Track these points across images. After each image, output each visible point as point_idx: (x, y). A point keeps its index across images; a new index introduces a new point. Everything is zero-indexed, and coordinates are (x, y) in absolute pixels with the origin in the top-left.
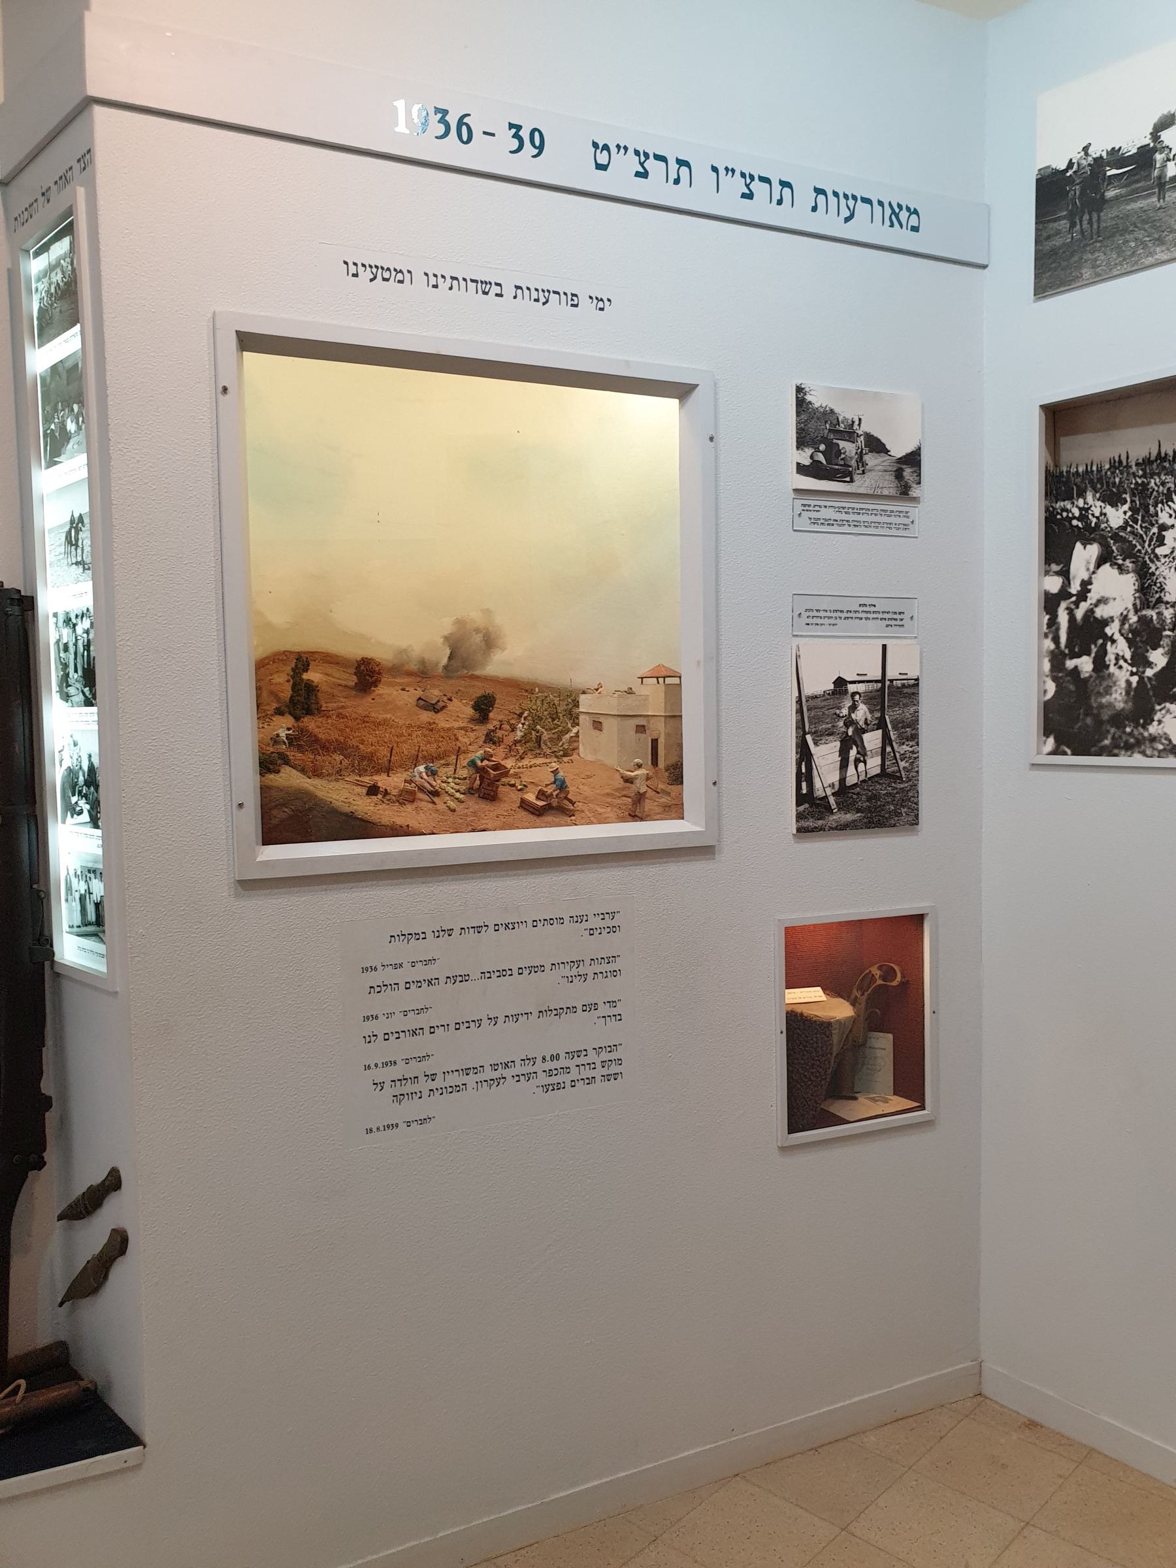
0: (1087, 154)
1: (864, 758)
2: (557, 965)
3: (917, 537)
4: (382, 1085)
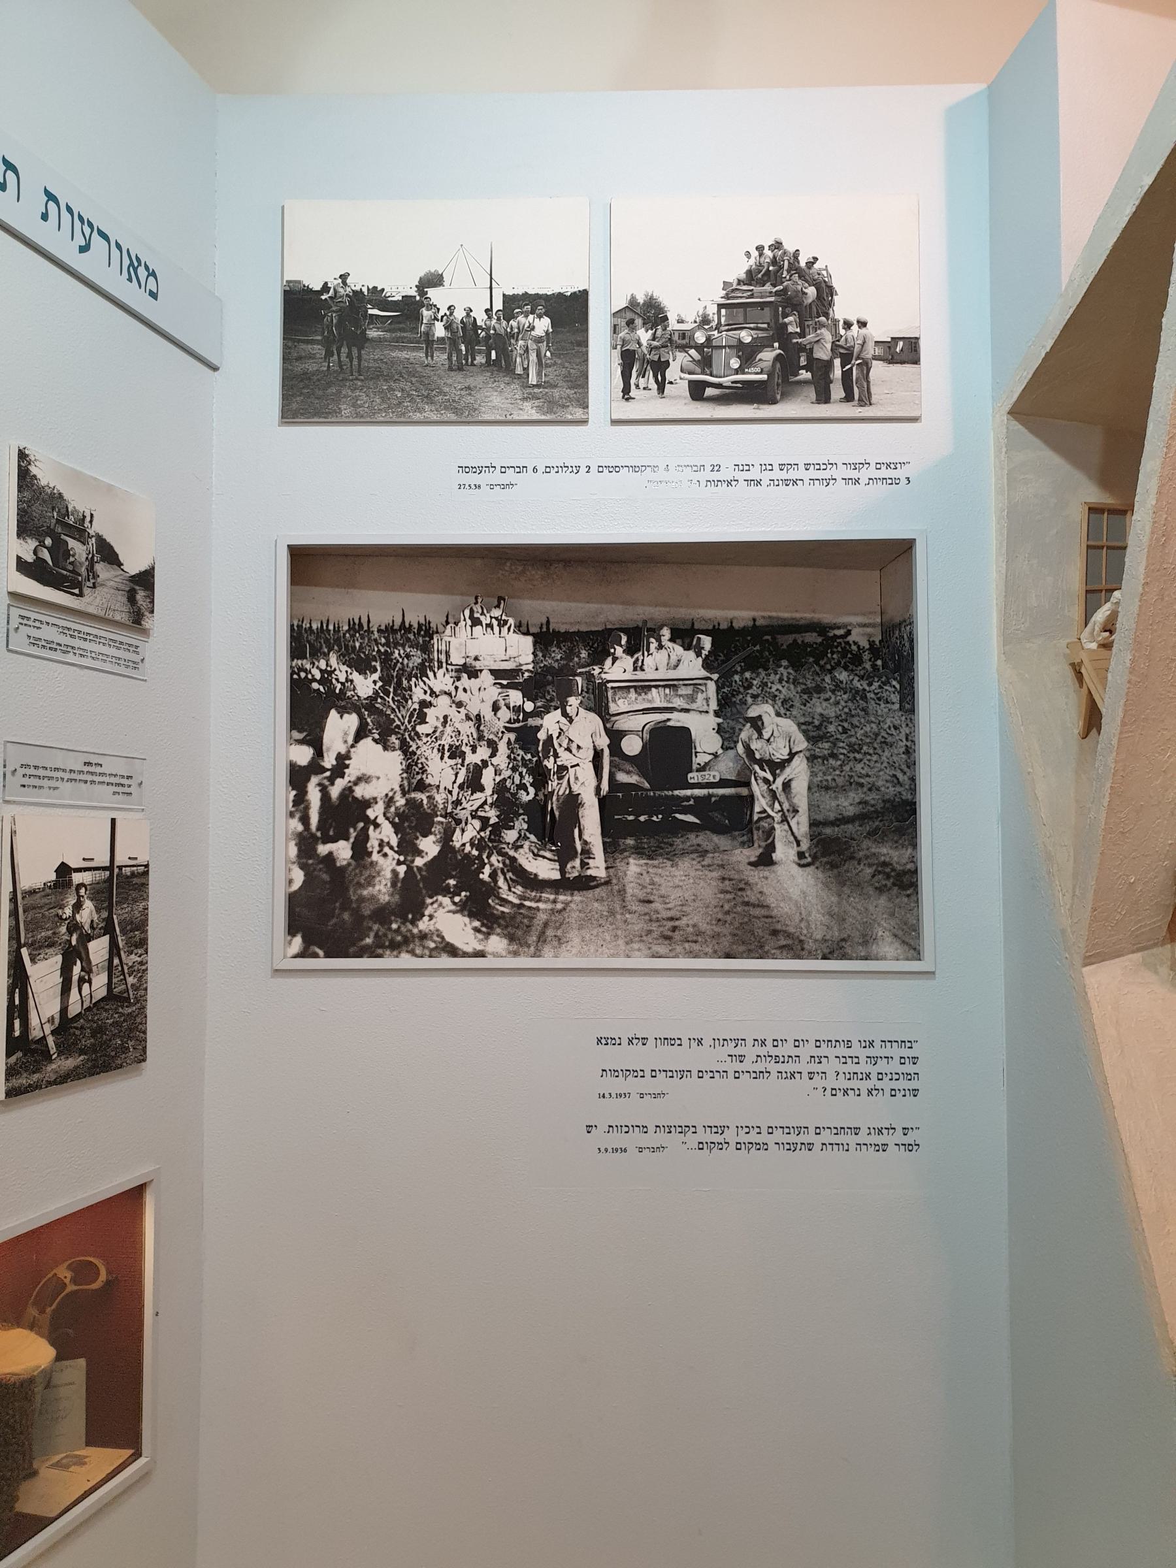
0: (344, 283)
1: (89, 976)
3: (146, 680)
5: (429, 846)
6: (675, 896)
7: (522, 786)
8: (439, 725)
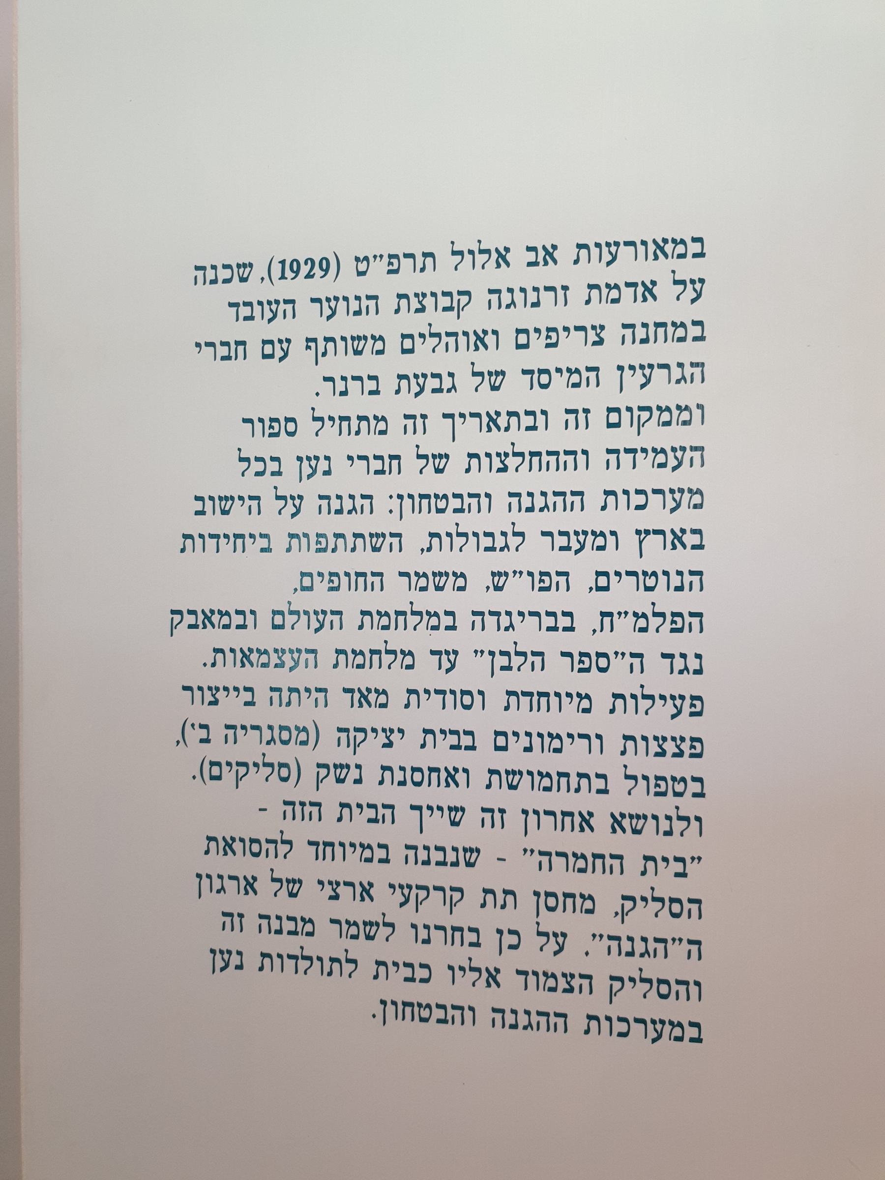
2: (419, 418)
4: (297, 502)
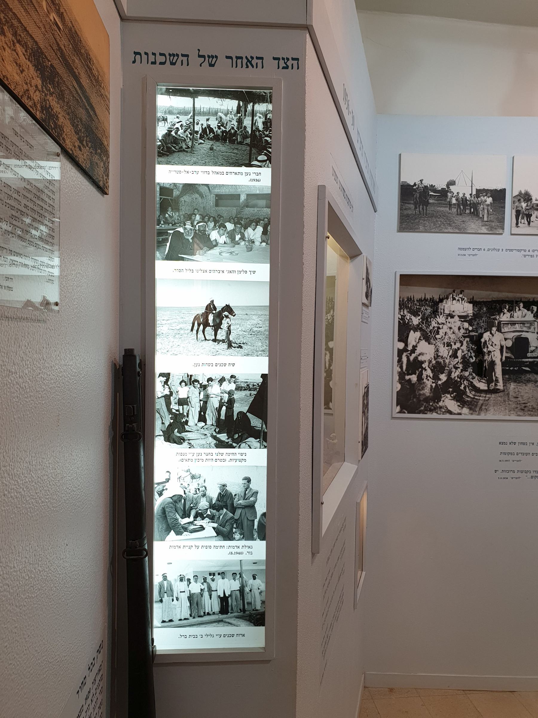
0: (421, 183)
5: (443, 377)
6: (526, 396)
7: (471, 357)
8: (443, 335)
